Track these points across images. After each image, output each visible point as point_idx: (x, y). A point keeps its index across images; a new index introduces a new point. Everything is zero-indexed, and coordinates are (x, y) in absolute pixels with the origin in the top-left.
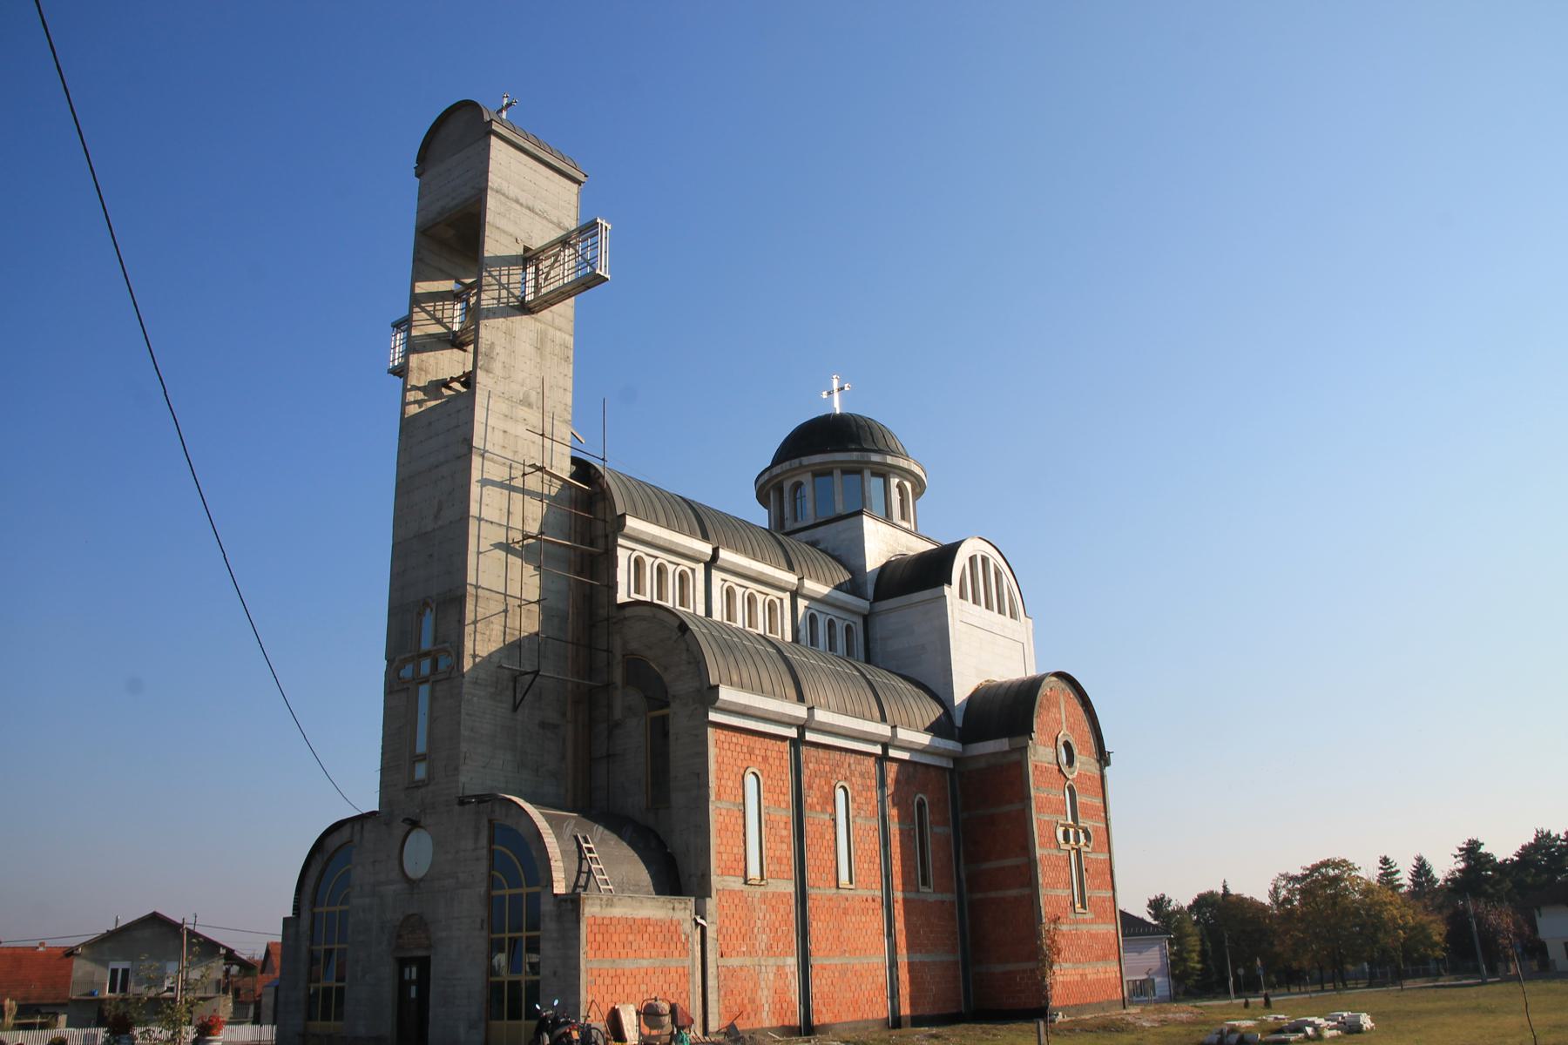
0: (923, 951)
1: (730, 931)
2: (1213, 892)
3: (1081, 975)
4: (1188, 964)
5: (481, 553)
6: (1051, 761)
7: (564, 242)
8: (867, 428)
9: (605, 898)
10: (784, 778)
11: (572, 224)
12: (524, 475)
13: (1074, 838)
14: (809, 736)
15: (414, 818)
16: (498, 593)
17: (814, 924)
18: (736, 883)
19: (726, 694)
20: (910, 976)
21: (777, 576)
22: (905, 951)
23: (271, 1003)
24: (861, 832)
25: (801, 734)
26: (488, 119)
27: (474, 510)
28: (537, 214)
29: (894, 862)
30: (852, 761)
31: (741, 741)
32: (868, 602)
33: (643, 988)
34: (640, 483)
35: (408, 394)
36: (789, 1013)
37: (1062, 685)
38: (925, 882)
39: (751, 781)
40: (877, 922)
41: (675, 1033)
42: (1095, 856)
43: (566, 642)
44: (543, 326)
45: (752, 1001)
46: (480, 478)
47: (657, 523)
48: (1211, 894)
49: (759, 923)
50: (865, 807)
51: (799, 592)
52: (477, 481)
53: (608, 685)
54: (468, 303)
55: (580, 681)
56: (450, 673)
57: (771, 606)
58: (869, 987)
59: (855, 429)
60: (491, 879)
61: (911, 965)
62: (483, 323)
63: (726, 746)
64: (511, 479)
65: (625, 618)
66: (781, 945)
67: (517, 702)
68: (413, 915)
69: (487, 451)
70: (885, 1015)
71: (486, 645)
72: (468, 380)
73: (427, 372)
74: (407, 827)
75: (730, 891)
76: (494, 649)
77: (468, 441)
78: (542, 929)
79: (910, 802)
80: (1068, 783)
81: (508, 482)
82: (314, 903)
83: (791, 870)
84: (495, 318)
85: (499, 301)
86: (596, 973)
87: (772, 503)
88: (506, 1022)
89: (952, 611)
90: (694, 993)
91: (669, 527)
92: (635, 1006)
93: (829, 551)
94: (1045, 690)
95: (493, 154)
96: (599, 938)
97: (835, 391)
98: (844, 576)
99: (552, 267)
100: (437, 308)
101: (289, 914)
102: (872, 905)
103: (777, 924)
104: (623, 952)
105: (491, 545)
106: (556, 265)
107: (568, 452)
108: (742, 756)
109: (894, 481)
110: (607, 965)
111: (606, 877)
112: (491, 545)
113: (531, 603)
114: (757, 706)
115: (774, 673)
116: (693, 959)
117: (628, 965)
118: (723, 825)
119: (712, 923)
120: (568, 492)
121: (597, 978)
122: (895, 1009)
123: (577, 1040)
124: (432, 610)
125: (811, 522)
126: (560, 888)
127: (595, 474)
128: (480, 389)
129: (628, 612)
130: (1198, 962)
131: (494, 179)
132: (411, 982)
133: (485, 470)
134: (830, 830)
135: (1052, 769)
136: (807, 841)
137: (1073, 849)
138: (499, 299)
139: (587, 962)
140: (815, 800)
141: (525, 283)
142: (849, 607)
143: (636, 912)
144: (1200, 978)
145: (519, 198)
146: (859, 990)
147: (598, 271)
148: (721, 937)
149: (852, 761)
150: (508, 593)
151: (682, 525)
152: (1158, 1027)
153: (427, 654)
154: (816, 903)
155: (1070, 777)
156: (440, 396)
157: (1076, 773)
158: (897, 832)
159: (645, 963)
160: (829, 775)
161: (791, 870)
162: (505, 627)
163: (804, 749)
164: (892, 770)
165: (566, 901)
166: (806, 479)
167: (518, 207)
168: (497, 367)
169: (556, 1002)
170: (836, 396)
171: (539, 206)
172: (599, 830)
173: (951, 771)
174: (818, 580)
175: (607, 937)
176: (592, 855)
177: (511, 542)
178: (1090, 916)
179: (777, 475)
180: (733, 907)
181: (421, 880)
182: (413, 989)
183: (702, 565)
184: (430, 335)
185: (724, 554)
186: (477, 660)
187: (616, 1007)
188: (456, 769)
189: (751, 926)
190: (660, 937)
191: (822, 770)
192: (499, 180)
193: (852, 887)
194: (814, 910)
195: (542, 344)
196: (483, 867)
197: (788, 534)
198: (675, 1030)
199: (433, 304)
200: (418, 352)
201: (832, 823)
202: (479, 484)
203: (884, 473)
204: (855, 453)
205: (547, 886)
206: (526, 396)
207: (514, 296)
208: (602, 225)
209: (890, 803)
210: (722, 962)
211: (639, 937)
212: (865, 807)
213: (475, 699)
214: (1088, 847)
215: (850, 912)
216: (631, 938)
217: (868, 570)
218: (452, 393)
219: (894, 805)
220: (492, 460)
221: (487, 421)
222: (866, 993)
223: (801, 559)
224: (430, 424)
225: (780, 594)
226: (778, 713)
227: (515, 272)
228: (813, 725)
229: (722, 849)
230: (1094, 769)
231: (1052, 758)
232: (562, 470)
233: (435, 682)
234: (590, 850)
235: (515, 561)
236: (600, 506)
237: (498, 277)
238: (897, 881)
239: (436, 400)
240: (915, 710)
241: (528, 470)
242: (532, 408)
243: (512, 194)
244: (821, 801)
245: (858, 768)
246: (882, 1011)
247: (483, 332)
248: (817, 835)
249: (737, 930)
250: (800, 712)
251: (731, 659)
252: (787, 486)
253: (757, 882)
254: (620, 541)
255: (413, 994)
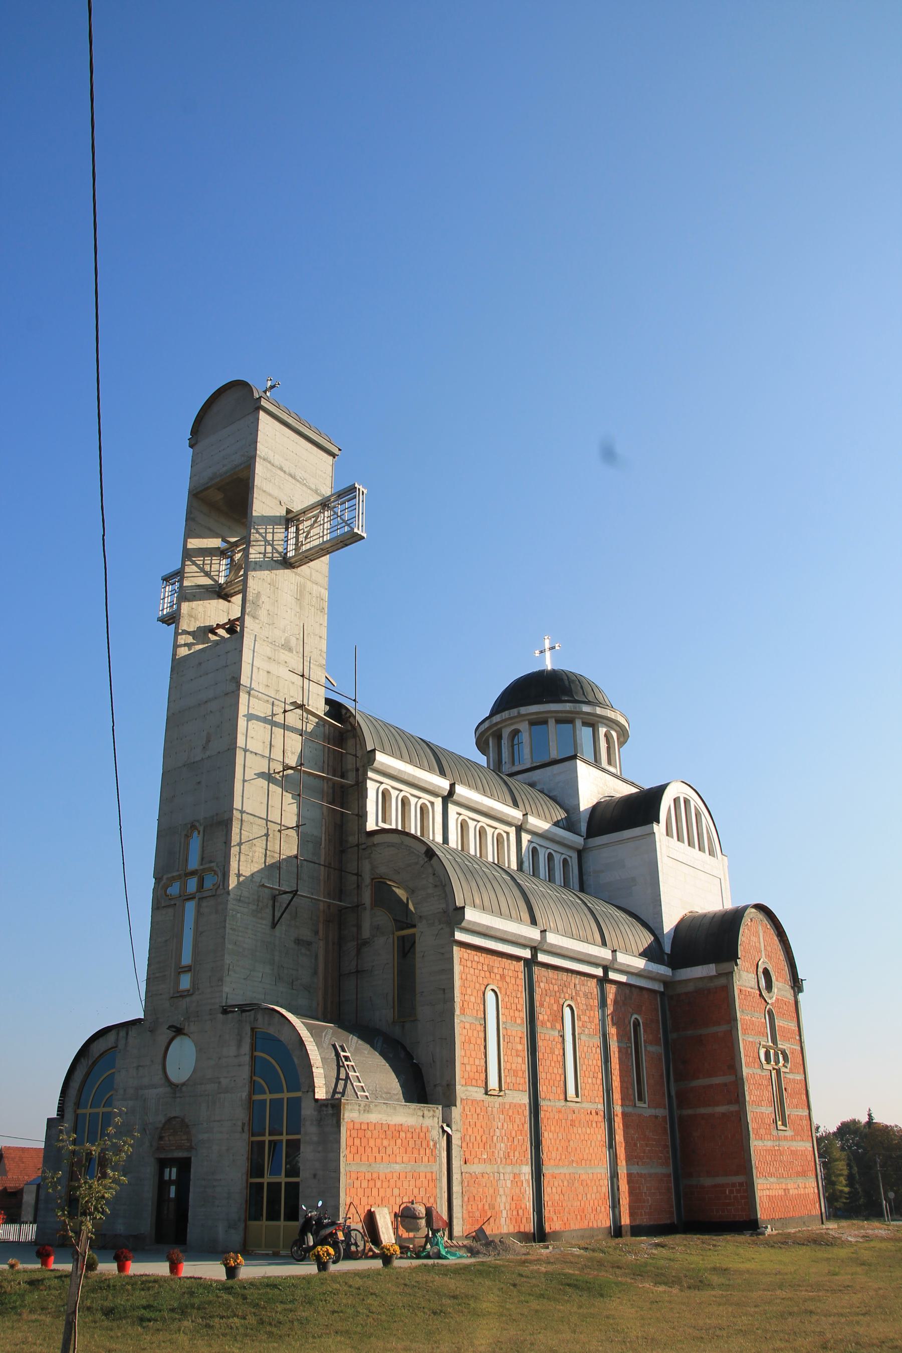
0: (640, 1163)
1: (473, 1139)
2: (855, 1120)
3: (785, 1190)
4: (836, 1187)
5: (246, 781)
6: (753, 986)
7: (324, 504)
8: (578, 683)
9: (363, 1104)
10: (519, 996)
11: (327, 491)
12: (285, 711)
13: (775, 1058)
14: (542, 958)
15: (178, 1026)
16: (261, 818)
17: (546, 1134)
18: (477, 1093)
19: (471, 915)
20: (629, 1187)
21: (505, 811)
22: (624, 1163)
23: (33, 1202)
24: (585, 1049)
25: (534, 955)
26: (258, 397)
27: (240, 742)
28: (298, 481)
29: (614, 1078)
30: (577, 982)
31: (482, 959)
32: (582, 838)
33: (396, 1191)
34: (386, 724)
35: (179, 637)
36: (524, 1220)
37: (760, 916)
38: (641, 1098)
39: (490, 997)
40: (601, 1134)
41: (430, 1236)
42: (791, 1076)
43: (319, 864)
44: (302, 580)
45: (492, 1207)
46: (246, 713)
47: (401, 758)
48: (854, 1122)
49: (498, 1132)
50: (589, 1025)
51: (523, 826)
52: (243, 716)
53: (358, 906)
54: (232, 560)
55: (332, 901)
56: (216, 890)
57: (499, 839)
58: (593, 1196)
59: (567, 683)
60: (253, 1083)
61: (630, 1176)
62: (251, 574)
63: (469, 964)
64: (273, 715)
65: (374, 845)
66: (517, 1154)
67: (276, 919)
68: (175, 1117)
69: (253, 689)
70: (608, 1225)
71: (249, 866)
72: (234, 628)
73: (196, 619)
74: (171, 1034)
75: (473, 1101)
76: (256, 870)
77: (236, 680)
78: (302, 1132)
79: (626, 1022)
80: (768, 1007)
81: (270, 718)
82: (78, 1105)
83: (525, 1082)
84: (261, 570)
85: (264, 556)
86: (354, 1176)
87: (491, 749)
88: (264, 1223)
89: (660, 846)
90: (441, 1198)
91: (411, 762)
92: (389, 1209)
93: (546, 791)
94: (746, 920)
95: (261, 426)
96: (357, 1142)
97: (547, 650)
98: (561, 815)
99: (312, 526)
100: (206, 562)
101: (54, 1114)
102: (596, 1118)
103: (514, 1134)
104: (379, 1157)
105: (255, 774)
106: (316, 525)
107: (322, 692)
108: (482, 974)
109: (602, 730)
110: (363, 1169)
111: (362, 1084)
112: (255, 774)
113: (288, 828)
114: (498, 927)
115: (510, 899)
116: (440, 1165)
117: (383, 1169)
118: (467, 1037)
119: (457, 1130)
120: (322, 728)
121: (356, 1181)
122: (616, 1219)
123: (342, 1241)
124: (199, 832)
125: (528, 766)
126: (321, 1093)
127: (346, 714)
128: (248, 633)
129: (377, 839)
130: (846, 1186)
131: (262, 448)
132: (171, 1182)
133: (250, 705)
134: (559, 1046)
135: (754, 993)
136: (540, 1055)
137: (774, 1069)
138: (265, 553)
139: (346, 1165)
140: (546, 1017)
141: (287, 541)
142: (566, 842)
143: (390, 1118)
144: (848, 1201)
145: (283, 466)
146: (585, 1199)
147: (356, 530)
148: (464, 1145)
149: (577, 982)
150: (269, 819)
151: (423, 762)
152: (864, 1242)
153: (193, 873)
154: (548, 1114)
155: (769, 1001)
156: (206, 640)
157: (774, 998)
158: (616, 1050)
159: (397, 1167)
160: (558, 994)
161: (525, 1082)
162: (266, 850)
163: (536, 969)
164: (611, 990)
165: (326, 1106)
166: (524, 727)
167: (282, 474)
168: (262, 613)
169: (320, 1204)
170: (548, 654)
171: (299, 474)
172: (354, 1040)
173: (662, 994)
174: (539, 816)
175: (364, 1141)
176: (348, 1063)
177: (272, 772)
178: (789, 1133)
179: (497, 724)
180: (475, 1116)
181: (183, 1084)
182: (173, 1189)
183: (440, 799)
184: (199, 586)
185: (460, 789)
186: (241, 879)
187: (372, 1210)
188: (221, 980)
189: (491, 1135)
190: (411, 1143)
191: (551, 989)
192: (266, 450)
193: (578, 1100)
194: (545, 1121)
195: (300, 595)
196: (245, 1072)
197: (511, 775)
198: (430, 1233)
199: (202, 559)
200: (189, 601)
201: (561, 1039)
202: (246, 719)
203: (592, 723)
204: (568, 704)
205: (307, 1092)
206: (287, 641)
207: (278, 552)
208: (359, 489)
209: (610, 1023)
210: (465, 1168)
211: (392, 1143)
212: (589, 1025)
213: (239, 915)
214: (787, 1067)
215: (577, 1122)
216: (385, 1143)
217: (581, 810)
218: (218, 638)
219: (613, 1024)
220: (257, 697)
221: (253, 662)
222: (592, 1202)
223: (524, 797)
224: (200, 664)
225: (507, 828)
226: (515, 934)
227: (279, 531)
228: (545, 947)
229: (466, 1060)
230: (789, 994)
231: (753, 983)
232: (317, 708)
233: (201, 899)
234: (347, 1058)
235: (276, 790)
236: (350, 742)
237: (264, 535)
238: (617, 1096)
239: (203, 644)
240: (631, 937)
241: (288, 707)
242: (292, 653)
243: (277, 463)
244: (551, 1019)
245: (583, 988)
246: (605, 1221)
247: (251, 582)
248: (548, 1050)
249: (478, 1138)
250: (534, 934)
251: (474, 884)
252: (506, 733)
253: (496, 1093)
254: (370, 774)
255: (172, 1195)
